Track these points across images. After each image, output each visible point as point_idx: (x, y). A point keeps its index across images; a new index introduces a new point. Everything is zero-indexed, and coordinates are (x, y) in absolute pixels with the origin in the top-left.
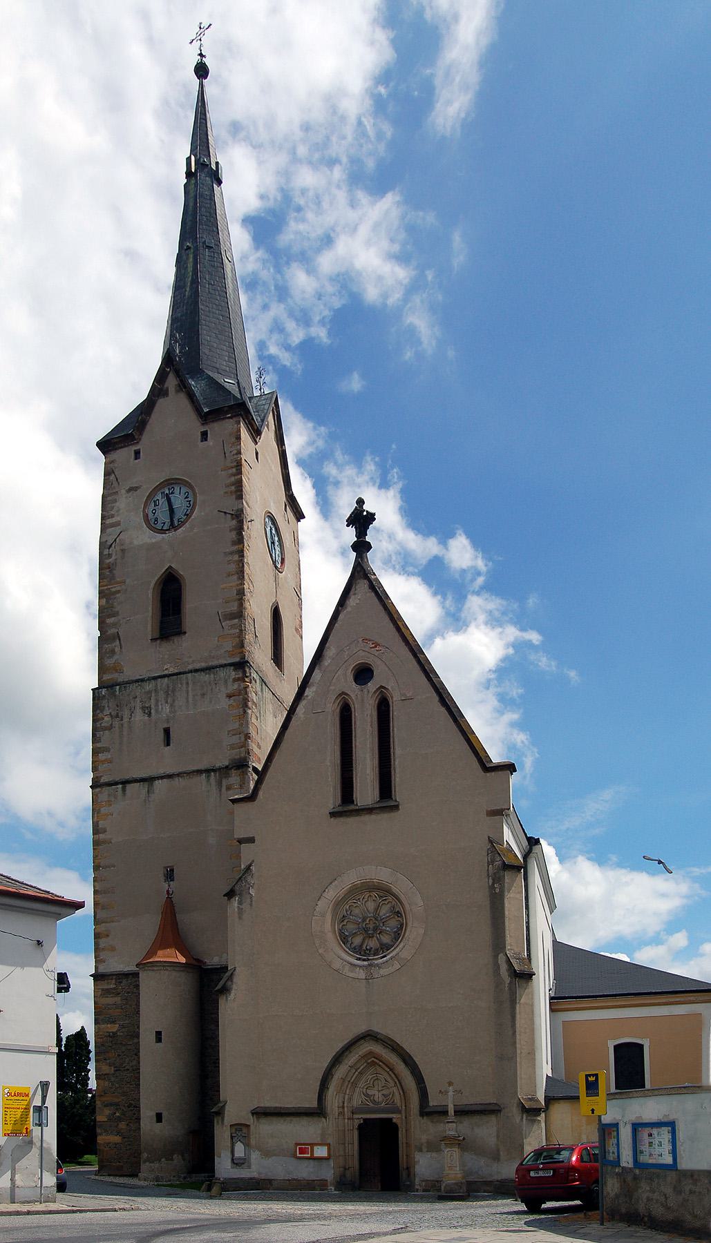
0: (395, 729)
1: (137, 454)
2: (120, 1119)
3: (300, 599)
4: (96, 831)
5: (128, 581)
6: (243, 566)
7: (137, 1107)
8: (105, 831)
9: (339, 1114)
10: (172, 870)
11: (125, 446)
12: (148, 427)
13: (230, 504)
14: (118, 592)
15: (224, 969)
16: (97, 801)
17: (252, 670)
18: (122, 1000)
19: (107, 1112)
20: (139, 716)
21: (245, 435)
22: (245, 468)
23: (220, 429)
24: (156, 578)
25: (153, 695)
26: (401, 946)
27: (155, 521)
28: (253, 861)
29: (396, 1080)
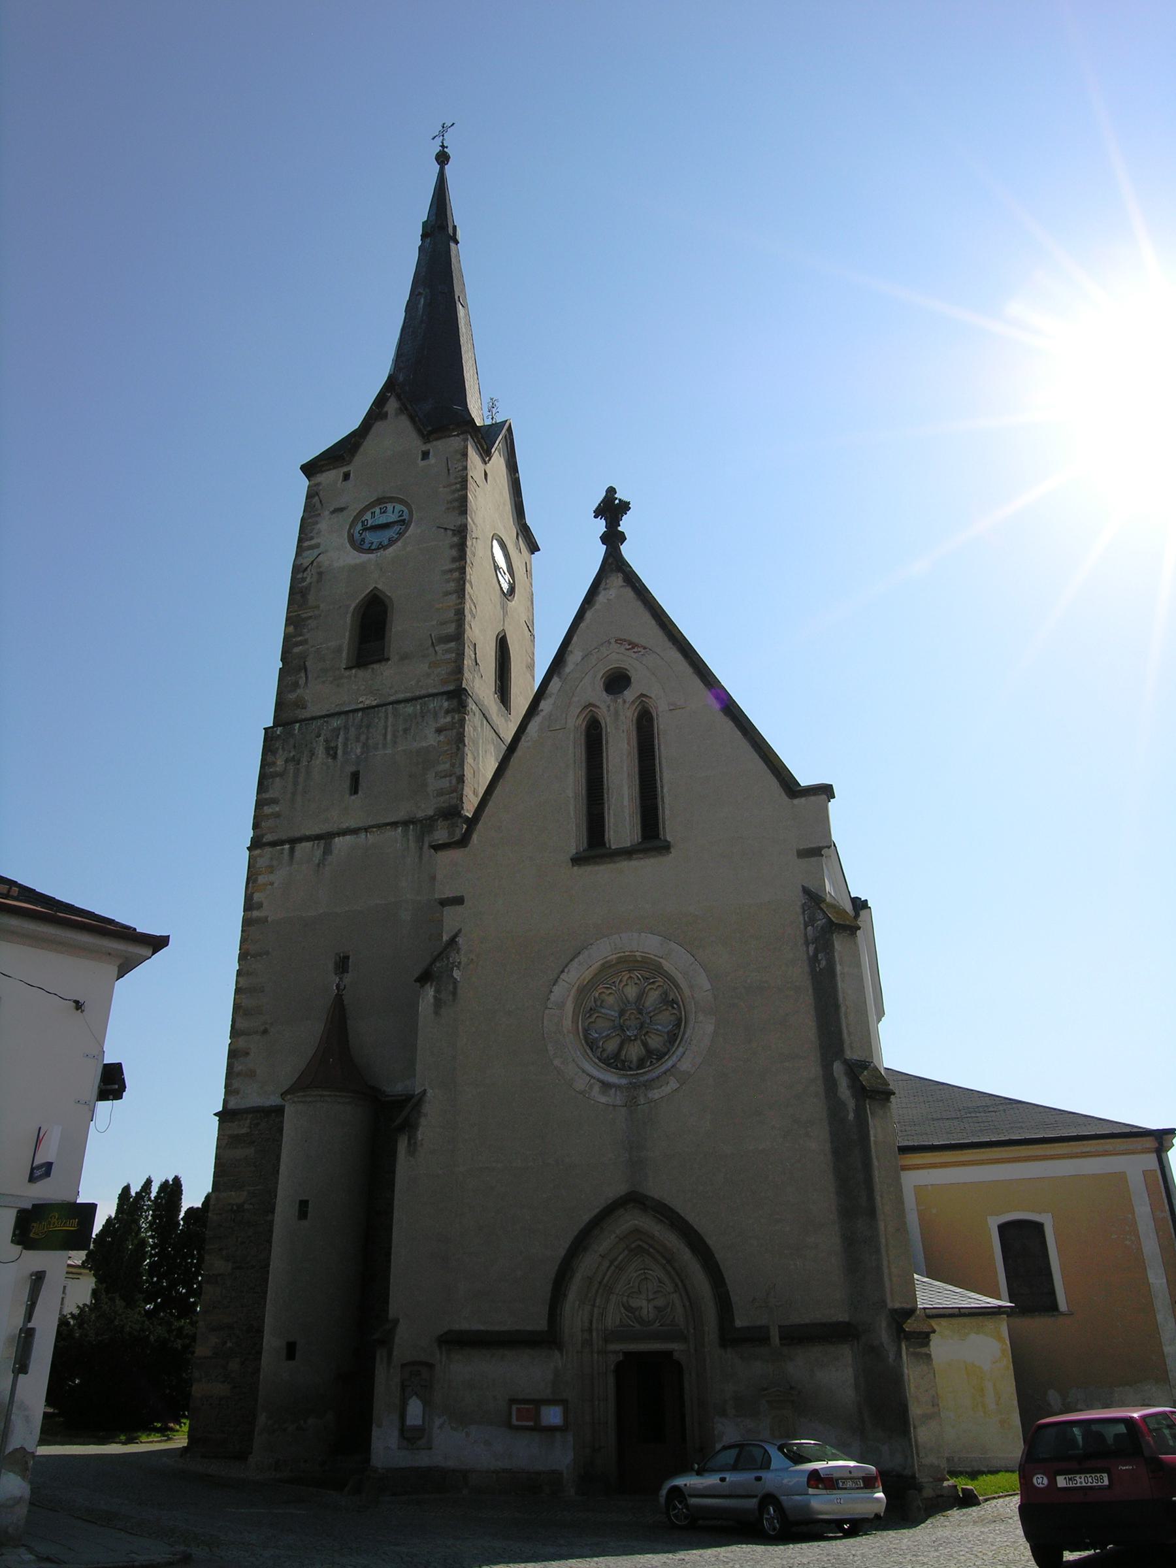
1: (346, 477)
3: (533, 635)
4: (249, 905)
5: (322, 606)
6: (464, 583)
8: (260, 906)
11: (334, 468)
12: (362, 449)
13: (453, 521)
14: (310, 617)
15: (409, 1098)
21: (473, 456)
22: (471, 485)
23: (443, 447)
24: (357, 601)
26: (678, 1053)
27: (362, 541)
28: (460, 931)
29: (678, 1281)
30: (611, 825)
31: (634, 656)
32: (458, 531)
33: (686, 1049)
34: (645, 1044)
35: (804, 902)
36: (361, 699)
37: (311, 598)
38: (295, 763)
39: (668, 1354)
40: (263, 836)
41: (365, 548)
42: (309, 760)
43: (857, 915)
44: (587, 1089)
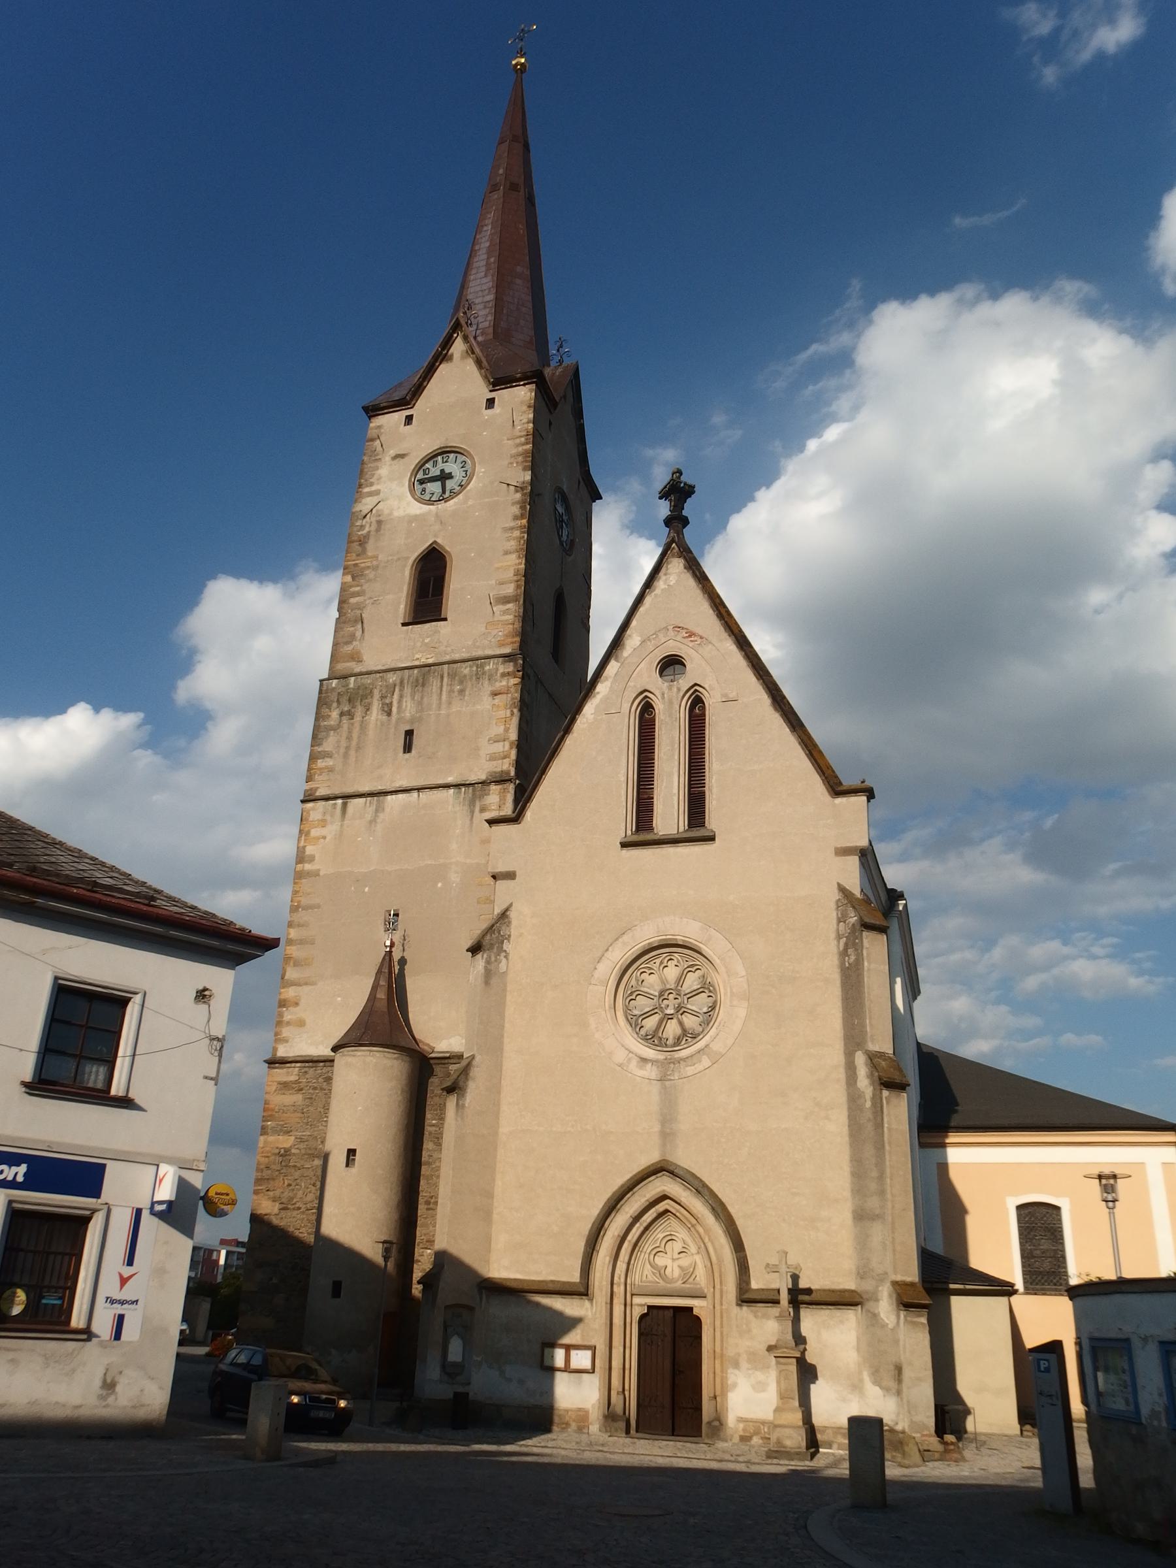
1: (409, 419)
5: (380, 557)
8: (312, 859)
14: (368, 567)
20: (375, 714)
25: (397, 690)
27: (423, 491)
28: (511, 905)
31: (691, 644)
32: (521, 488)
33: (720, 1031)
34: (681, 1023)
36: (417, 656)
39: (690, 1309)
41: (425, 498)
44: (625, 1062)
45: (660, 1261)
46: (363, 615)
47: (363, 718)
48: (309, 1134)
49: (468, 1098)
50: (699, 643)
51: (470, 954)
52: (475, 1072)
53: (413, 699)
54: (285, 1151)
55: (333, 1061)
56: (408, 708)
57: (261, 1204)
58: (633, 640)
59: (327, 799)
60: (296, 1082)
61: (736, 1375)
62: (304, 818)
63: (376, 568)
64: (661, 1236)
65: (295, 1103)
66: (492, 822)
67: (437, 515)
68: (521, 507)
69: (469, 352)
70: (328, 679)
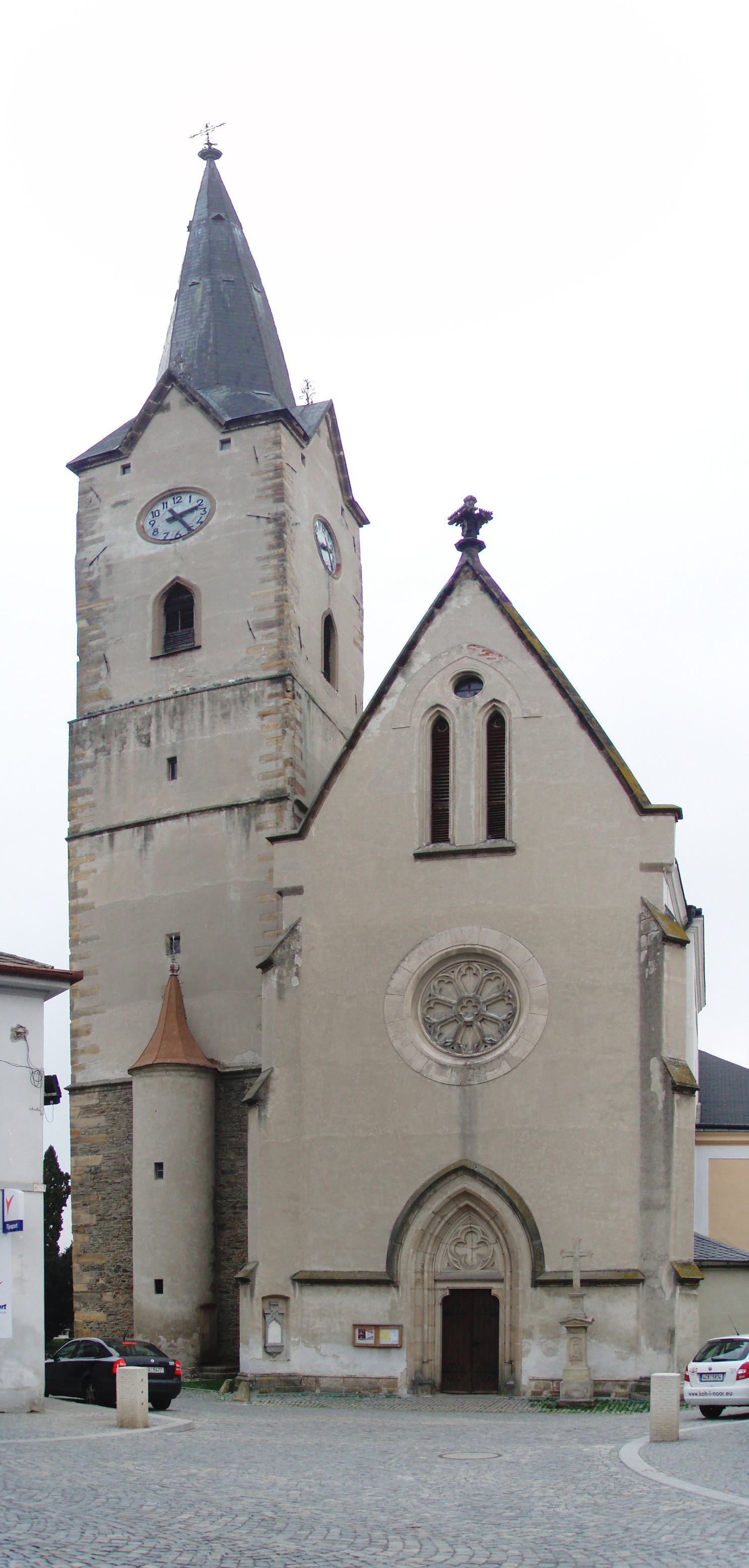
0: (513, 752)
2: (104, 1289)
4: (74, 893)
7: (128, 1272)
8: (85, 893)
9: (416, 1282)
10: (178, 938)
14: (104, 610)
16: (74, 856)
17: (296, 684)
18: (107, 1121)
19: (88, 1278)
20: (133, 746)
25: (154, 720)
27: (154, 532)
28: (300, 919)
30: (456, 823)
31: (488, 662)
35: (641, 912)
36: (172, 686)
37: (103, 590)
38: (106, 753)
40: (80, 825)
42: (121, 749)
43: (687, 925)
45: (461, 1251)
46: (107, 655)
47: (120, 752)
48: (115, 1151)
49: (269, 1109)
50: (497, 660)
51: (260, 970)
52: (273, 1084)
53: (172, 727)
54: (96, 1170)
55: (131, 1083)
56: (169, 737)
57: (80, 1217)
58: (421, 657)
59: (92, 834)
60: (97, 1105)
61: (530, 1344)
62: (71, 855)
63: (112, 610)
64: (462, 1228)
65: (99, 1124)
66: (273, 840)
67: (176, 552)
68: (276, 537)
69: (190, 400)
70: (77, 721)
